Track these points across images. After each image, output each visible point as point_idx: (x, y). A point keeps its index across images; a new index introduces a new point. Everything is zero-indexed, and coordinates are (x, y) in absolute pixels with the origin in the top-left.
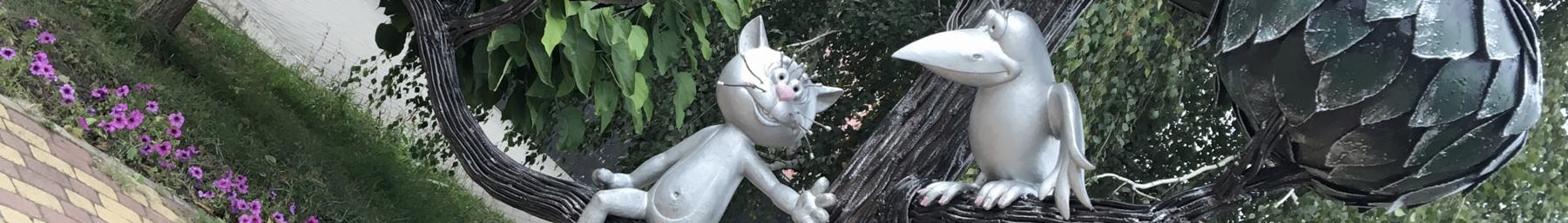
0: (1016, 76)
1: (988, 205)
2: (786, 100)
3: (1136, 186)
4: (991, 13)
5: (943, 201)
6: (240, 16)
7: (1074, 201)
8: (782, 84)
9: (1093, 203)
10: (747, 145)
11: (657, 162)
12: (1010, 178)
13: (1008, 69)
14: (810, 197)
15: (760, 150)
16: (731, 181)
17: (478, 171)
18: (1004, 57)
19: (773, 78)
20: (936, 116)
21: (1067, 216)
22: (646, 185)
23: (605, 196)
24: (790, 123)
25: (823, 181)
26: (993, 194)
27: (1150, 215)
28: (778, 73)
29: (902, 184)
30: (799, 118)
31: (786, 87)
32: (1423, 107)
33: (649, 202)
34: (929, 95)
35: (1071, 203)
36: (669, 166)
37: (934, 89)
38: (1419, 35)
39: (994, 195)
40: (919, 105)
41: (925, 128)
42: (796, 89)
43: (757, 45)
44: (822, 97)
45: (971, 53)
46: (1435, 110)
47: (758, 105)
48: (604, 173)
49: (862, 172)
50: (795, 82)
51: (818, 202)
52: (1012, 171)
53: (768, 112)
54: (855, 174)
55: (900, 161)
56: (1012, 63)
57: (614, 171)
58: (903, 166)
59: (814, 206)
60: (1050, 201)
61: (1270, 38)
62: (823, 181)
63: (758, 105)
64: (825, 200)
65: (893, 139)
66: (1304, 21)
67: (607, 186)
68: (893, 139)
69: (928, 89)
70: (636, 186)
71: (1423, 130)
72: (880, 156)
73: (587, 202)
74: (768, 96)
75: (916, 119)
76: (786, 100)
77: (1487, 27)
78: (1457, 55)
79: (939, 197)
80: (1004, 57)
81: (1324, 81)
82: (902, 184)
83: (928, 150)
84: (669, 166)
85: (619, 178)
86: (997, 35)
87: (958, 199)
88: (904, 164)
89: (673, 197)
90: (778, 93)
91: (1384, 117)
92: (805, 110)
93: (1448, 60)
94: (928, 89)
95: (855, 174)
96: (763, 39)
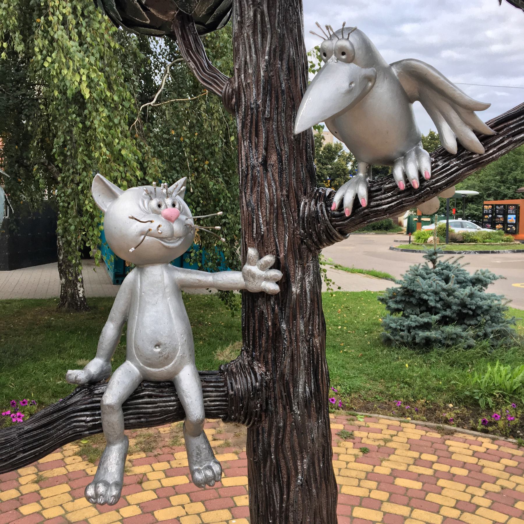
3: (152, 103)
5: (364, 202)
11: (110, 330)
15: (181, 262)
19: (154, 212)
24: (187, 228)
28: (154, 203)
33: (139, 368)
35: (481, 140)
39: (413, 174)
40: (266, 149)
42: (174, 205)
47: (162, 239)
51: (262, 268)
52: (401, 149)
53: (172, 236)
54: (263, 228)
55: (288, 196)
58: (293, 198)
59: (263, 273)
62: (252, 252)
63: (162, 239)
64: (267, 263)
68: (269, 185)
88: (291, 195)
89: (158, 350)
95: (263, 228)
96: (114, 188)
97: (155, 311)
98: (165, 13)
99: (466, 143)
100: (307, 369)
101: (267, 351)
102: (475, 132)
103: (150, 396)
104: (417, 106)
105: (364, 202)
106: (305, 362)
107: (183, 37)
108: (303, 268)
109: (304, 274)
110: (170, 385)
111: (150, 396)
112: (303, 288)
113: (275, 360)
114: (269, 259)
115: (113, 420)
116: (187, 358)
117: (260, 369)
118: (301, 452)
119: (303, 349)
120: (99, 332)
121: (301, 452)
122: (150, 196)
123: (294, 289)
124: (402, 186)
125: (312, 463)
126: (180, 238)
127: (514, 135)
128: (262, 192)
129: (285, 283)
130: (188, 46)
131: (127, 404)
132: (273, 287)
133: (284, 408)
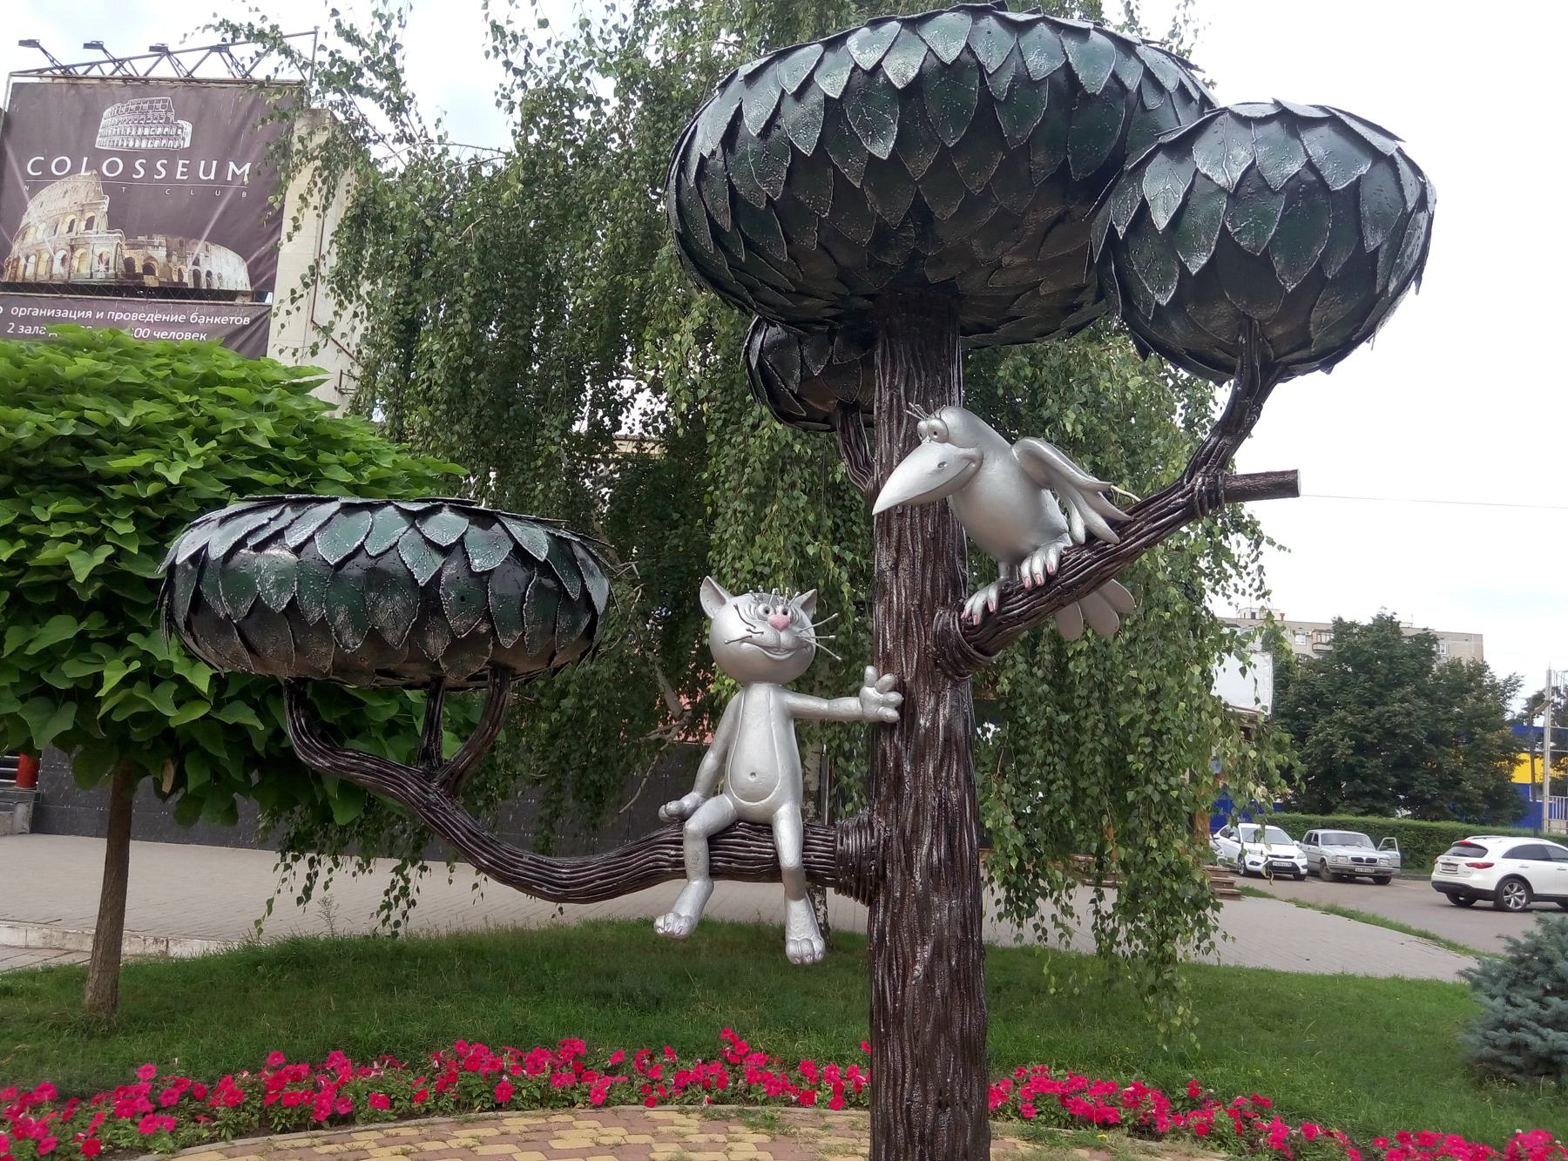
0: (980, 461)
1: (1040, 580)
2: (785, 627)
4: (922, 424)
5: (993, 607)
6: (163, 948)
7: (1113, 523)
8: (771, 617)
9: (1130, 514)
10: (777, 689)
11: (709, 761)
12: (1036, 548)
13: (971, 459)
14: (869, 691)
15: (803, 684)
16: (787, 727)
17: (560, 892)
18: (962, 451)
19: (760, 617)
20: (920, 548)
21: (1116, 539)
22: (714, 790)
23: (692, 825)
24: (800, 644)
25: (870, 670)
26: (1035, 568)
27: (1188, 487)
28: (761, 609)
29: (938, 625)
30: (804, 635)
31: (776, 616)
32: (1367, 232)
34: (900, 536)
36: (723, 758)
37: (900, 530)
38: (1325, 173)
40: (898, 551)
41: (918, 565)
43: (723, 602)
44: (805, 607)
45: (934, 465)
46: (1377, 227)
47: (765, 648)
48: (672, 806)
49: (895, 639)
50: (780, 609)
52: (1033, 541)
53: (777, 648)
55: (920, 606)
56: (971, 451)
57: (679, 798)
58: (925, 609)
60: (1091, 536)
61: (1204, 261)
63: (765, 648)
65: (899, 594)
66: (1224, 225)
67: (683, 817)
68: (899, 594)
69: (895, 533)
70: (706, 797)
71: (1377, 249)
72: (899, 615)
73: (681, 843)
74: (768, 636)
75: (905, 562)
76: (785, 627)
77: (302, 540)
78: (1364, 170)
79: (986, 607)
80: (962, 451)
81: (1278, 261)
82: (938, 625)
83: (934, 580)
84: (723, 758)
85: (687, 801)
86: (944, 437)
87: (1003, 598)
90: (774, 626)
91: (1343, 260)
92: (803, 626)
93: (1359, 178)
94: (895, 533)
96: (725, 594)
97: (758, 744)
98: (823, 403)
99: (1096, 531)
100: (936, 828)
101: (889, 800)
102: (1104, 517)
103: (744, 837)
104: (1047, 495)
105: (993, 607)
106: (933, 817)
107: (843, 430)
108: (938, 697)
109: (937, 704)
110: (764, 827)
111: (744, 837)
112: (935, 722)
113: (897, 810)
114: (888, 678)
115: (695, 852)
116: (789, 795)
117: (880, 823)
118: (923, 934)
119: (932, 800)
120: (697, 767)
121: (923, 934)
122: (759, 601)
123: (922, 722)
124: (1027, 583)
125: (937, 953)
126: (789, 650)
127: (1154, 521)
128: (891, 602)
129: (907, 709)
130: (847, 442)
131: (715, 839)
132: (891, 714)
133: (903, 874)
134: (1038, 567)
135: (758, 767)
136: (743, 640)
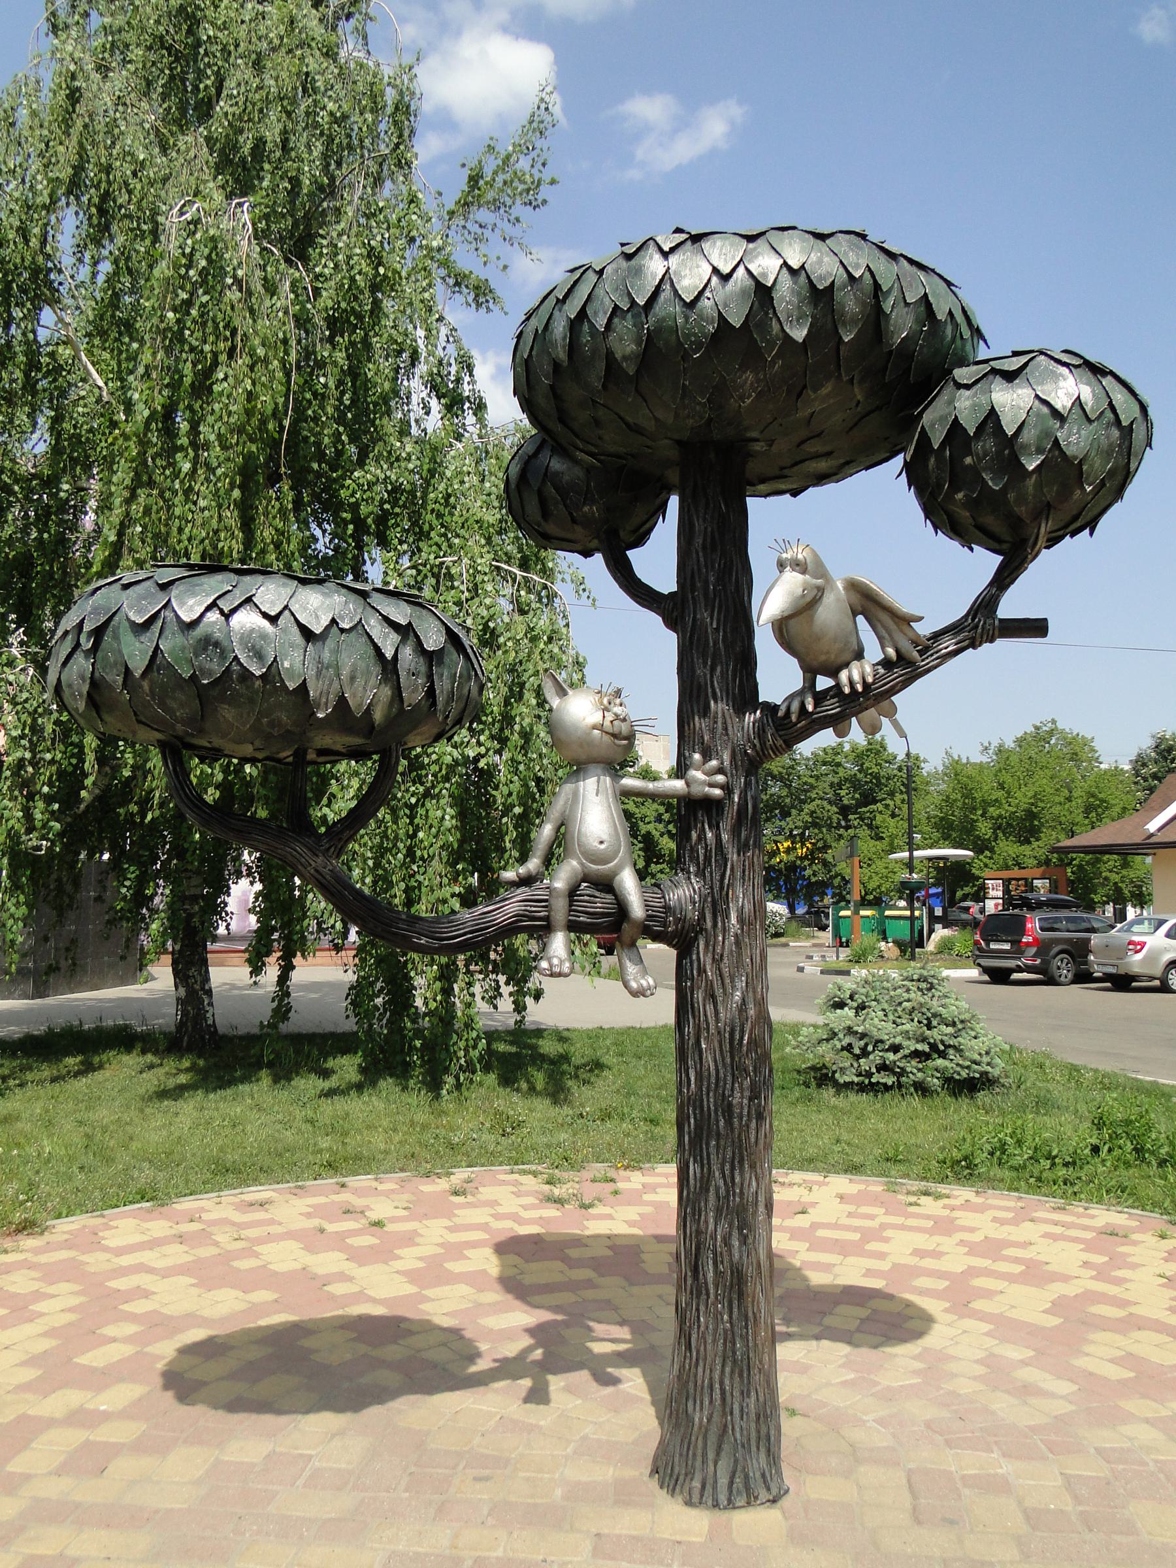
110: (606, 885)
134: (856, 677)
135: (605, 837)
136: (594, 727)
